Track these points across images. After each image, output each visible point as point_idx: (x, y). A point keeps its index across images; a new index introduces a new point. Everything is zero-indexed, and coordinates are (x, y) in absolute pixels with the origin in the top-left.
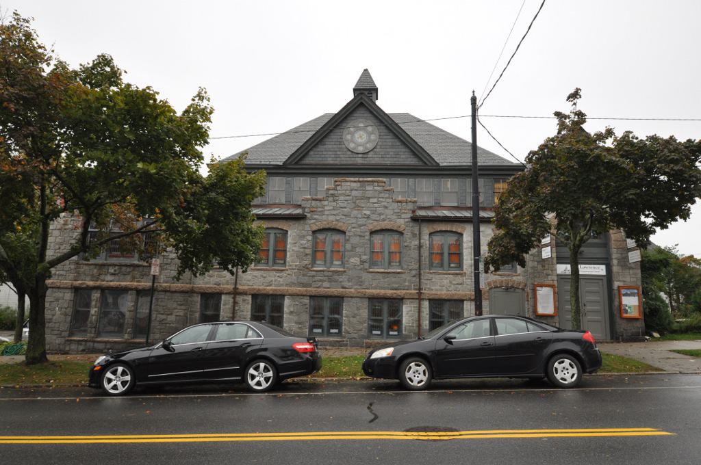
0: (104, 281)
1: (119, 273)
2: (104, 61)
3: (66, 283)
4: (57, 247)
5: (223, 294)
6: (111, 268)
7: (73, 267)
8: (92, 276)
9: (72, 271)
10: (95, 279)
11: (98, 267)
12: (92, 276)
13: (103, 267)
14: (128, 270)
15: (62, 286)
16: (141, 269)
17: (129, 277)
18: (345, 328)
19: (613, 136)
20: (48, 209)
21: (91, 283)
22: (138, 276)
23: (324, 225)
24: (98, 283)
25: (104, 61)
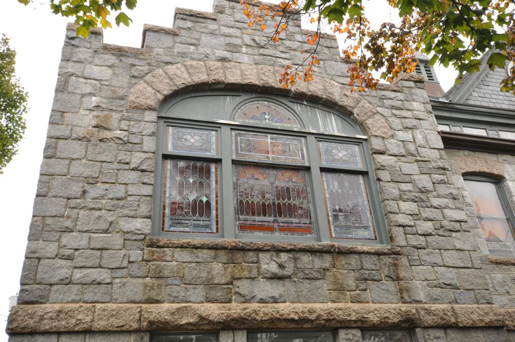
0: (247, 300)
1: (295, 274)
2: (177, 8)
3: (115, 315)
4: (76, 189)
5: (420, 327)
6: (264, 258)
7: (136, 255)
8: (209, 284)
9: (134, 269)
10: (219, 294)
11: (222, 253)
12: (209, 284)
13: (239, 256)
14: (318, 263)
15: (100, 325)
16: (354, 260)
17: (324, 286)
18: (479, 55)
19: (383, 30)
20: (353, 199)
21: (214, 311)
22: (351, 283)
23: (184, 78)
24: (236, 309)
25: (177, 8)
